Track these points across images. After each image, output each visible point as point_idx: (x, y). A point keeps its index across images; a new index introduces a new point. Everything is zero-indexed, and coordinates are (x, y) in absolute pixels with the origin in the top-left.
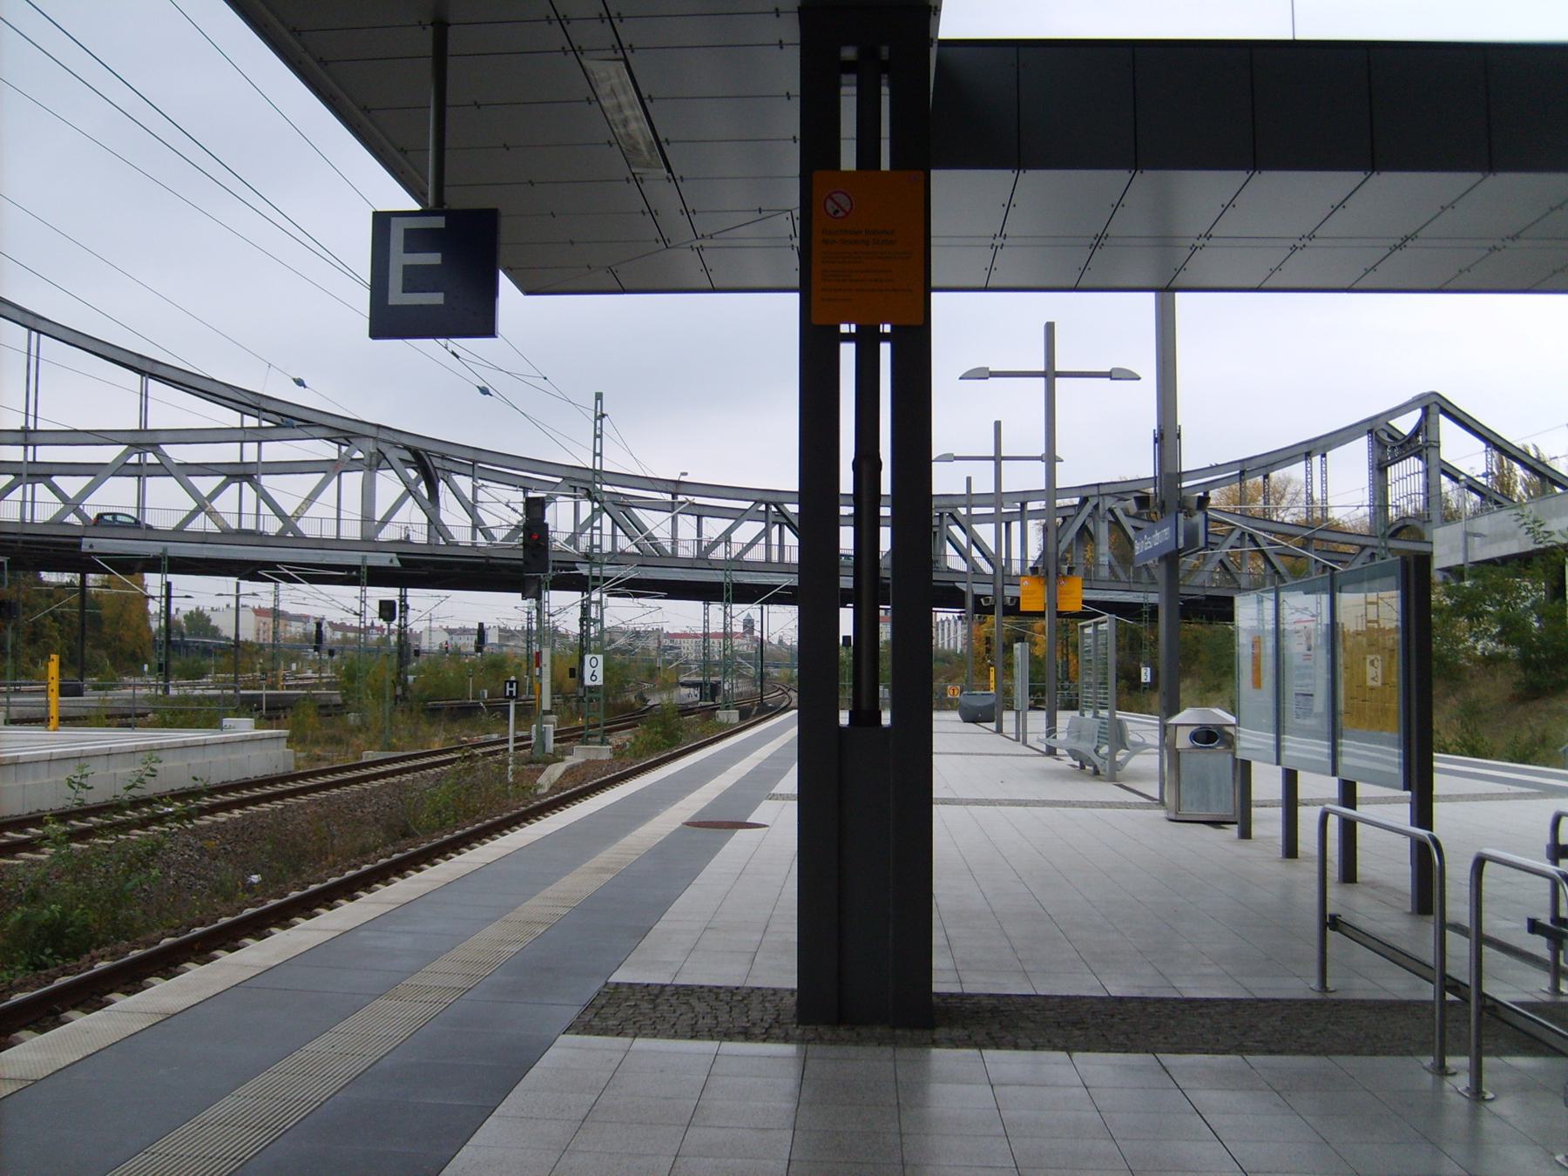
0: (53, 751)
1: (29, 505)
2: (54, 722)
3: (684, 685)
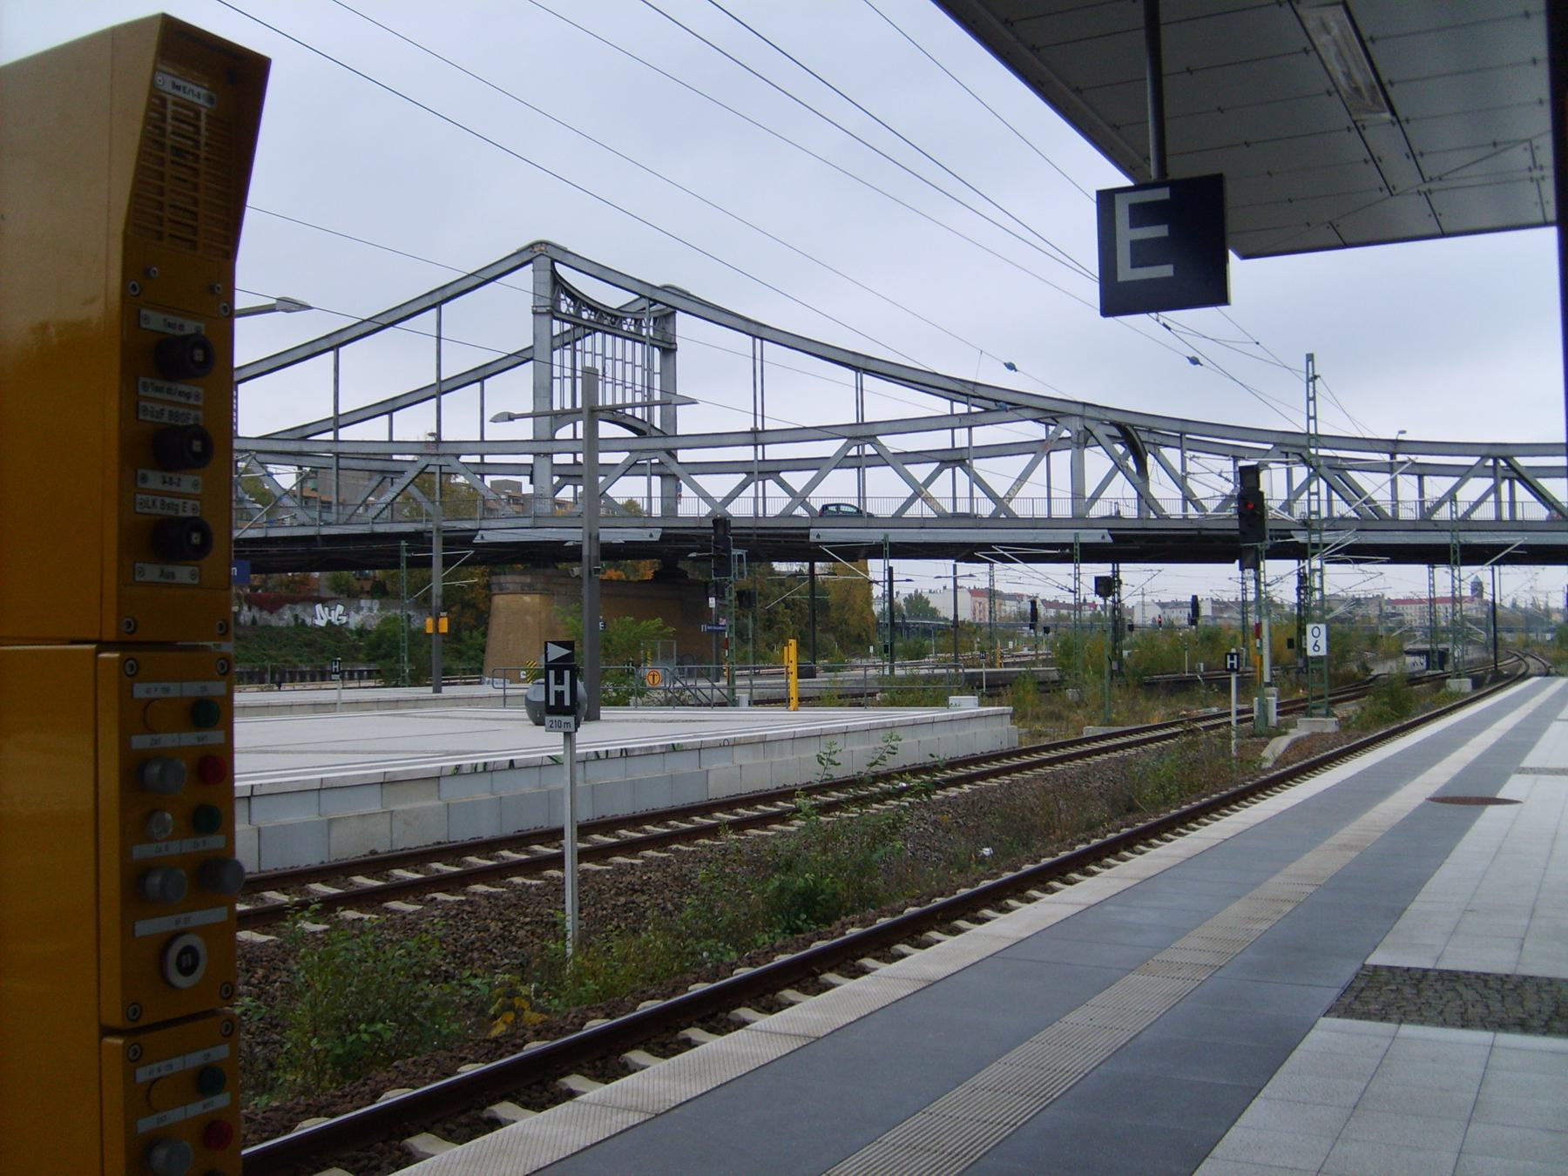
1: (760, 501)
2: (794, 702)
3: (1409, 653)
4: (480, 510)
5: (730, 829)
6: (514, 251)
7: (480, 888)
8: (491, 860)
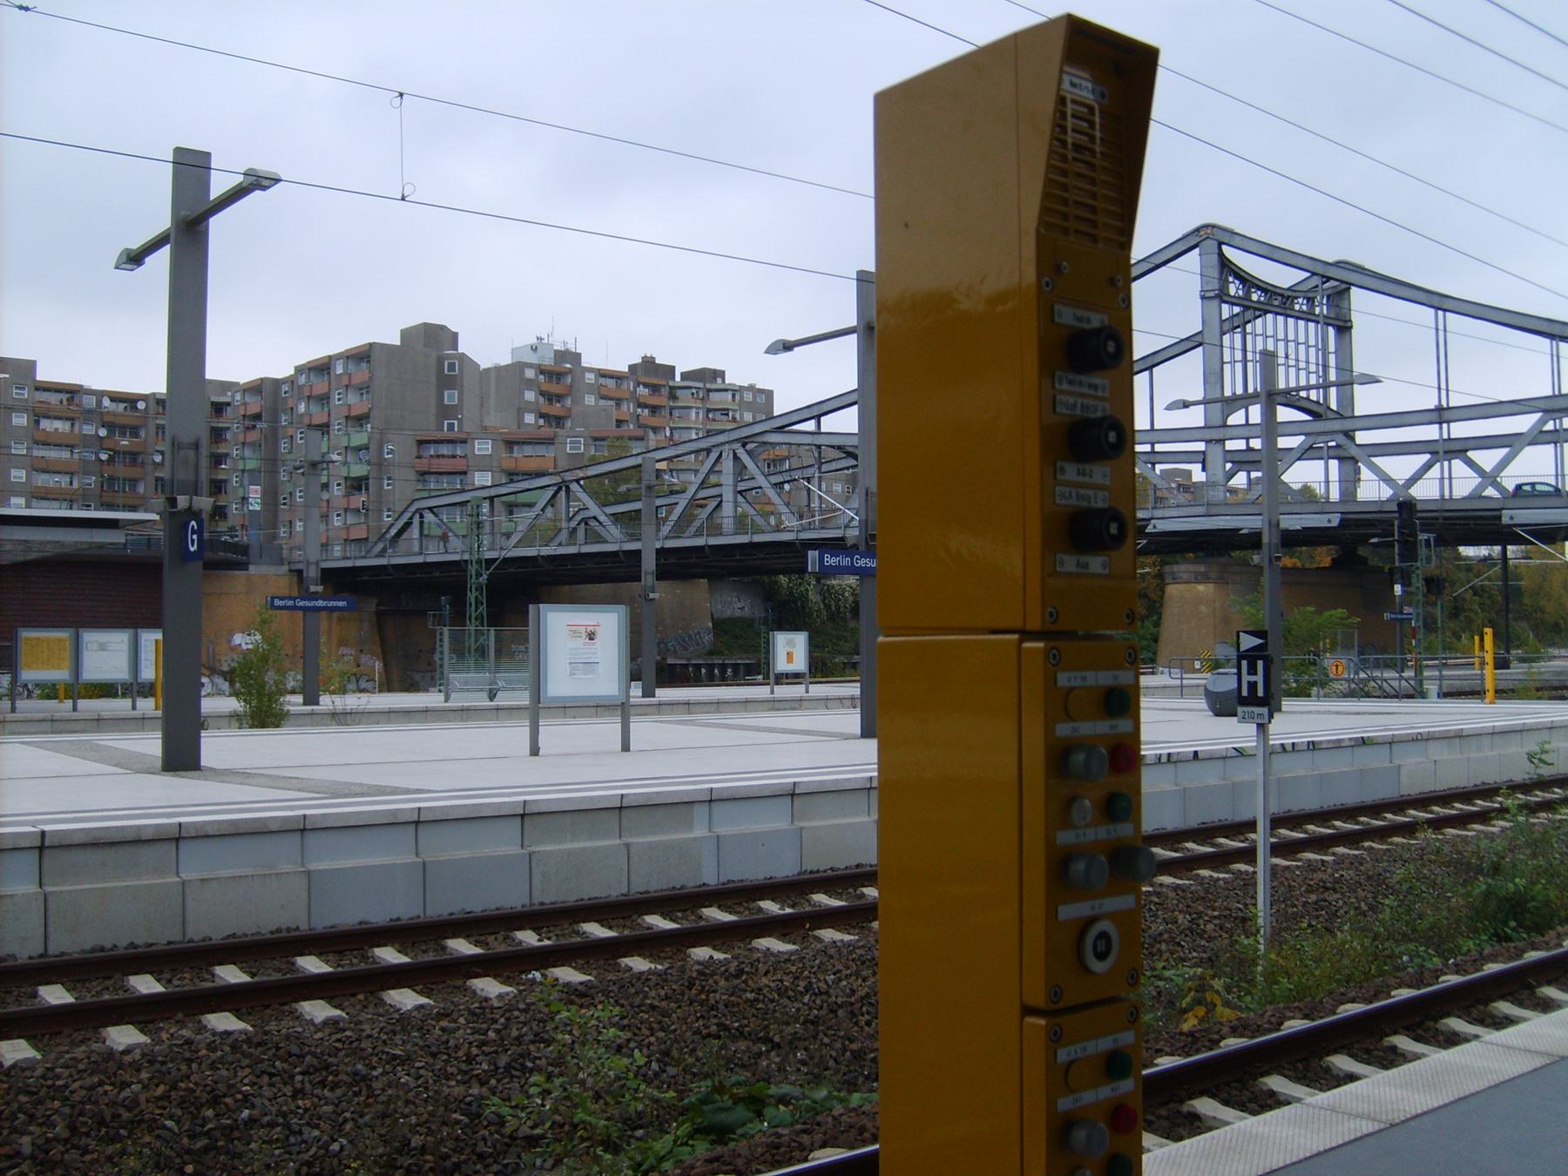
0: (1496, 724)
1: (1446, 482)
2: (1490, 695)
4: (1151, 499)
5: (1429, 827)
6: (1180, 236)
7: (1167, 880)
8: (1175, 851)
